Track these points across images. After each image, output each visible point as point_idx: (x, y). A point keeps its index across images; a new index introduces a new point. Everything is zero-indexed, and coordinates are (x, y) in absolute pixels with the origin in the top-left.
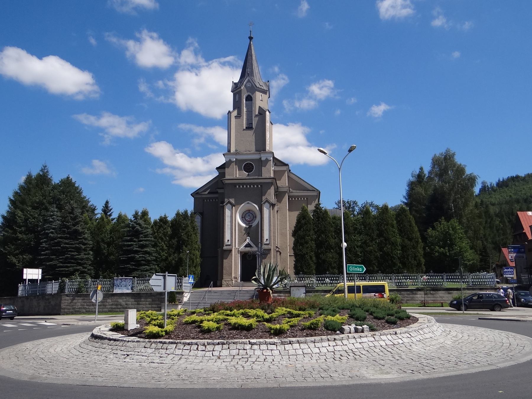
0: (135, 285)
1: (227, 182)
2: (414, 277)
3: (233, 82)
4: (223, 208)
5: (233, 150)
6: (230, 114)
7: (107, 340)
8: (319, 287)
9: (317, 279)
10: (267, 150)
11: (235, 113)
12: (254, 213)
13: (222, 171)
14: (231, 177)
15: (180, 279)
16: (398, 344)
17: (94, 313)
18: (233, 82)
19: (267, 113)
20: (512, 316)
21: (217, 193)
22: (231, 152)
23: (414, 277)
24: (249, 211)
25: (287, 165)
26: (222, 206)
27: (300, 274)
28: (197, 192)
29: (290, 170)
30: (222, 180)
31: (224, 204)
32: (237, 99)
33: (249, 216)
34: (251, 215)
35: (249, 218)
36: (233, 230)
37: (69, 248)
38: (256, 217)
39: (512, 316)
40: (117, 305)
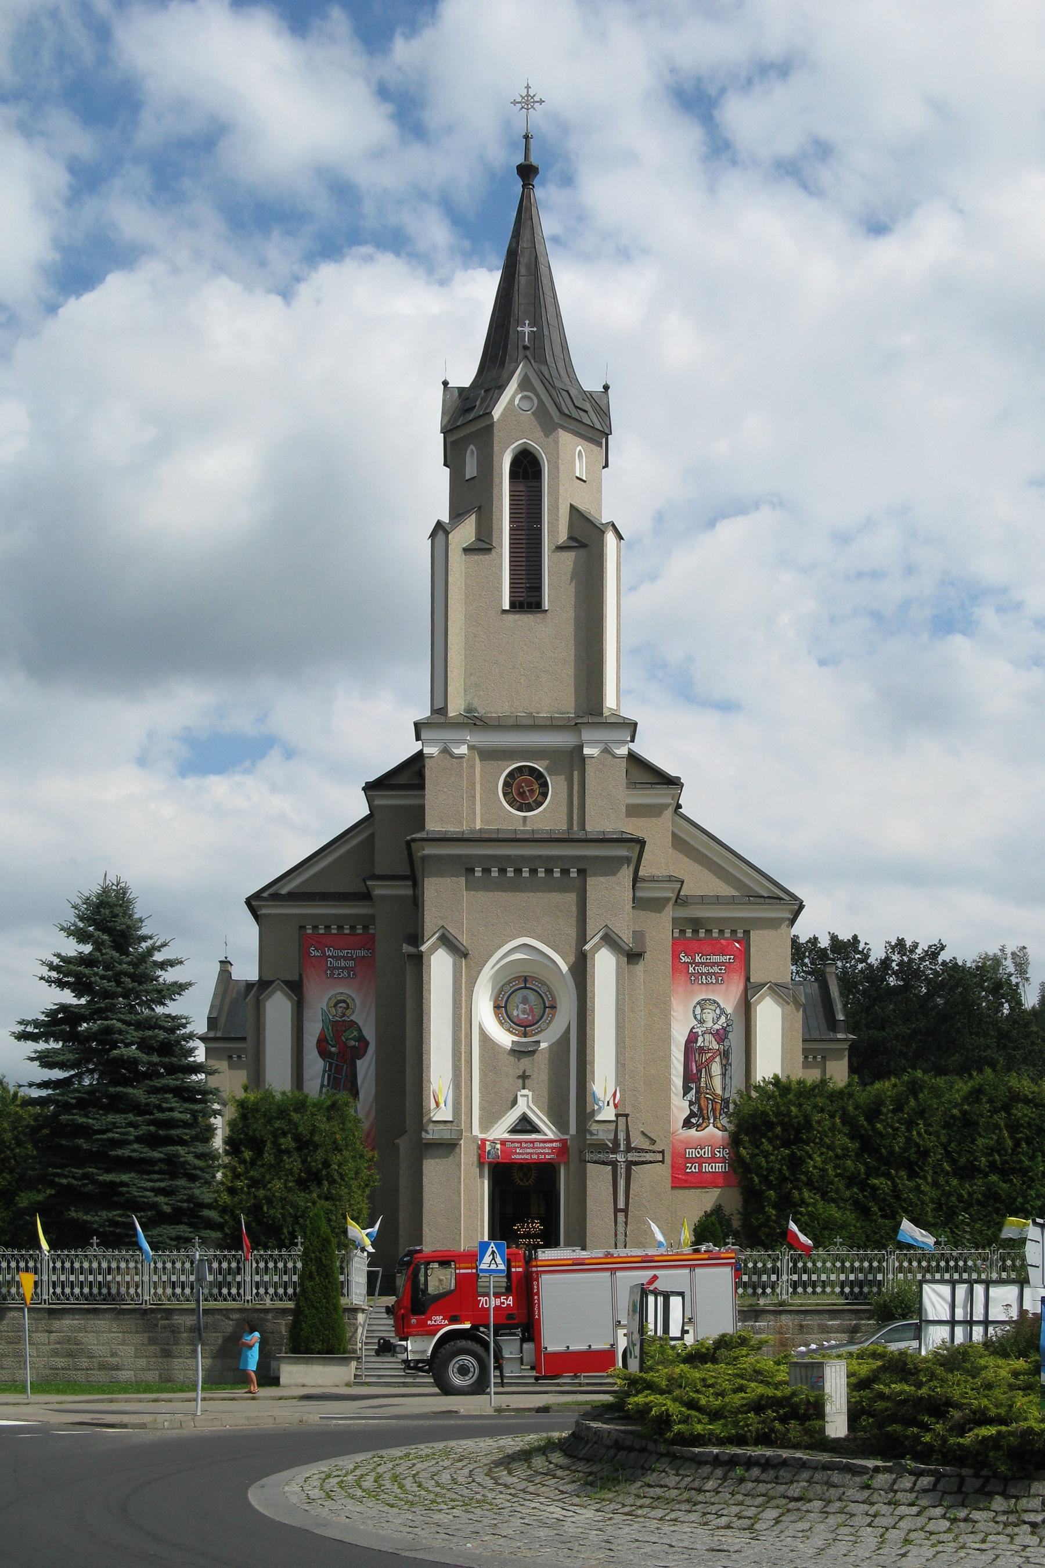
0: (146, 1278)
1: (430, 850)
2: (861, 1261)
3: (445, 383)
4: (418, 961)
5: (456, 707)
6: (441, 535)
7: (942, 1531)
8: (828, 1294)
9: (795, 1265)
10: (606, 713)
11: (466, 533)
12: (544, 989)
13: (387, 800)
14: (451, 828)
15: (67, 1255)
16: (896, 1523)
17: (23, 1391)
18: (445, 383)
19: (610, 538)
20: (403, 1396)
21: (366, 896)
22: (451, 714)
23: (861, 1261)
24: (525, 979)
25: (673, 783)
26: (411, 956)
27: (835, 1244)
28: (271, 891)
29: (679, 806)
30: (414, 840)
31: (423, 948)
32: (471, 469)
33: (525, 1001)
34: (532, 997)
35: (524, 1012)
36: (460, 1060)
37: (178, 1127)
38: (553, 1007)
39: (403, 1396)
40: (70, 1355)
